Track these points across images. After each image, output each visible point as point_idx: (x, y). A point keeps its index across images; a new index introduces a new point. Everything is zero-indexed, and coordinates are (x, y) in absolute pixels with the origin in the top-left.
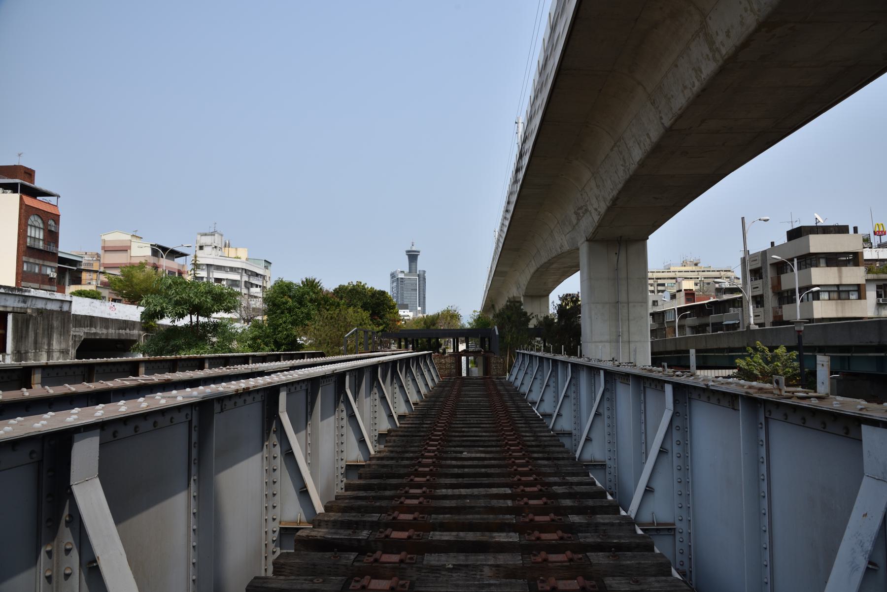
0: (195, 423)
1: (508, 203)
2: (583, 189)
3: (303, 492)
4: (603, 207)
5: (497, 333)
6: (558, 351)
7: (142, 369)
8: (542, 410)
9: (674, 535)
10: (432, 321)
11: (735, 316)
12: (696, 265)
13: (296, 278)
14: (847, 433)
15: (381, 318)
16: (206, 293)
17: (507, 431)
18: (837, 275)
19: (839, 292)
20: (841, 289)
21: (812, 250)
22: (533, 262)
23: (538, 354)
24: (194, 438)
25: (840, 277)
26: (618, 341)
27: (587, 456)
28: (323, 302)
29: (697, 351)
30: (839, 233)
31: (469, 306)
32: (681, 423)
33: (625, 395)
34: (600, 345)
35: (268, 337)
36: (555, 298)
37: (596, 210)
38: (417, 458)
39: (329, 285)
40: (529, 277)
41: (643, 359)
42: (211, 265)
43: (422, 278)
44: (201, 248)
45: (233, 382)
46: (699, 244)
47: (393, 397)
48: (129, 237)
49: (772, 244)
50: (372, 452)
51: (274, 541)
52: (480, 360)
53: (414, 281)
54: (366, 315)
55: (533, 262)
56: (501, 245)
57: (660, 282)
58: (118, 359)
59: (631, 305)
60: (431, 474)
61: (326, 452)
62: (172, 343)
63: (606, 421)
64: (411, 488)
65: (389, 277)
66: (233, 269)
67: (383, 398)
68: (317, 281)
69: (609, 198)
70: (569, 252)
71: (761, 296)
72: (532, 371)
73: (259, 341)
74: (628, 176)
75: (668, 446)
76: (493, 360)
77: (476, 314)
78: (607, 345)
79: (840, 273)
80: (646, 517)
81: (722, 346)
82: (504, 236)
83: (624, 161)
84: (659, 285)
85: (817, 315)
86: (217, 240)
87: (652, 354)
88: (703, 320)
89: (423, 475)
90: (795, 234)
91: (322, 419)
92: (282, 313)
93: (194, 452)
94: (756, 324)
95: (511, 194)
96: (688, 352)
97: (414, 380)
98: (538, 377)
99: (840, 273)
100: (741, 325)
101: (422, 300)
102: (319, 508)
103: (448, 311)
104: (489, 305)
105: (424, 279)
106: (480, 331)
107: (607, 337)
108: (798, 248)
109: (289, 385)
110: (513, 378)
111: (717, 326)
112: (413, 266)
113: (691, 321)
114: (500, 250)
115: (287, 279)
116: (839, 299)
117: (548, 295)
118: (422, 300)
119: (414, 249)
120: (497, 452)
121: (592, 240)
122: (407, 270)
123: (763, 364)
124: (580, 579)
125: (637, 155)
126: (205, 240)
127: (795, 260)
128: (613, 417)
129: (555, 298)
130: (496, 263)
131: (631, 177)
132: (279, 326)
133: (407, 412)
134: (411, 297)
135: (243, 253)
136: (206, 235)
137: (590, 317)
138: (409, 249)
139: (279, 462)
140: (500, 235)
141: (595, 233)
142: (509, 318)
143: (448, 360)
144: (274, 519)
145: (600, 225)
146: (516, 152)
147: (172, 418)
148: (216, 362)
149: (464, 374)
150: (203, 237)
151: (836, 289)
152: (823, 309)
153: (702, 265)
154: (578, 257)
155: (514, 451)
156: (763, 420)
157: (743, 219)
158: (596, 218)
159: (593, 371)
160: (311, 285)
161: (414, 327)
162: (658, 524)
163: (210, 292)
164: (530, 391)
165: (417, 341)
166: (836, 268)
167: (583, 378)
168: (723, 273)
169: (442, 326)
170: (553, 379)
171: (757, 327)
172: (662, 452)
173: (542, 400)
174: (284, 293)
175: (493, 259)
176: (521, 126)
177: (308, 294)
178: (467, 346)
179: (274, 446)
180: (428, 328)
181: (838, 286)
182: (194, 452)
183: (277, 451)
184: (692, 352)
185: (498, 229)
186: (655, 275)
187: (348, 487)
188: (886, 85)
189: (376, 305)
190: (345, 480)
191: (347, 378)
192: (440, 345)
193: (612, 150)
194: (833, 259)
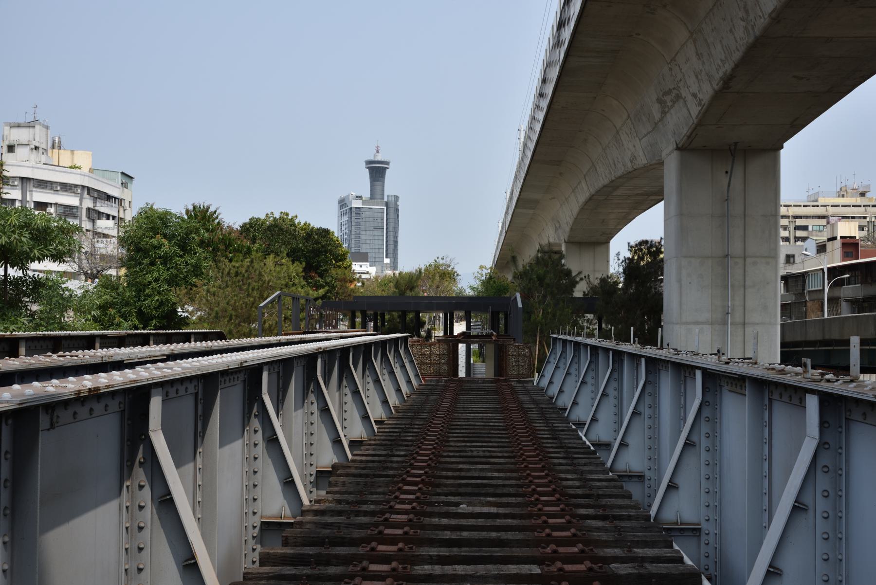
1: (544, 81)
4: (707, 92)
5: (520, 305)
12: (863, 194)
15: (321, 276)
16: (21, 227)
17: (535, 469)
22: (583, 184)
26: (725, 323)
28: (222, 247)
29: (863, 342)
31: (472, 263)
33: (736, 412)
35: (127, 304)
36: (620, 247)
37: (694, 95)
38: (383, 513)
40: (576, 210)
41: (763, 349)
42: (29, 179)
43: (392, 208)
44: (11, 148)
45: (71, 379)
47: (342, 410)
50: (306, 502)
55: (583, 184)
56: (529, 154)
57: (799, 222)
59: (748, 260)
60: (406, 539)
63: (704, 455)
64: (372, 562)
65: (336, 206)
66: (66, 187)
67: (325, 410)
68: (212, 209)
69: (718, 76)
70: (647, 169)
72: (565, 364)
73: (112, 311)
74: (751, 39)
75: (807, 500)
76: (511, 351)
77: (485, 271)
78: (707, 328)
82: (535, 138)
83: (747, 12)
84: (798, 228)
86: (38, 135)
89: (393, 541)
92: (152, 264)
95: (549, 65)
97: (377, 381)
101: (391, 247)
103: (437, 266)
104: (507, 256)
105: (397, 210)
106: (490, 302)
109: (166, 385)
110: (545, 382)
112: (379, 188)
113: (851, 291)
114: (527, 162)
115: (160, 205)
117: (607, 242)
118: (391, 247)
119: (379, 158)
120: (517, 505)
122: (366, 194)
126: (16, 136)
128: (715, 450)
129: (620, 247)
133: (364, 435)
135: (84, 159)
136: (19, 126)
137: (680, 281)
138: (371, 158)
139: (148, 516)
140: (528, 137)
141: (690, 137)
142: (541, 279)
143: (436, 350)
145: (701, 123)
146: (537, 76)
147: (75, 413)
148: (38, 345)
149: (462, 374)
150: (15, 131)
154: (662, 177)
158: (695, 110)
159: (683, 370)
160: (202, 216)
161: (379, 293)
162: (682, 524)
163: (27, 225)
164: (575, 403)
165: (383, 316)
169: (425, 291)
172: (798, 508)
173: (594, 420)
174: (155, 230)
175: (522, 159)
177: (197, 231)
178: (468, 327)
179: (141, 487)
180: (402, 293)
185: (524, 126)
186: (792, 211)
187: (265, 560)
189: (315, 252)
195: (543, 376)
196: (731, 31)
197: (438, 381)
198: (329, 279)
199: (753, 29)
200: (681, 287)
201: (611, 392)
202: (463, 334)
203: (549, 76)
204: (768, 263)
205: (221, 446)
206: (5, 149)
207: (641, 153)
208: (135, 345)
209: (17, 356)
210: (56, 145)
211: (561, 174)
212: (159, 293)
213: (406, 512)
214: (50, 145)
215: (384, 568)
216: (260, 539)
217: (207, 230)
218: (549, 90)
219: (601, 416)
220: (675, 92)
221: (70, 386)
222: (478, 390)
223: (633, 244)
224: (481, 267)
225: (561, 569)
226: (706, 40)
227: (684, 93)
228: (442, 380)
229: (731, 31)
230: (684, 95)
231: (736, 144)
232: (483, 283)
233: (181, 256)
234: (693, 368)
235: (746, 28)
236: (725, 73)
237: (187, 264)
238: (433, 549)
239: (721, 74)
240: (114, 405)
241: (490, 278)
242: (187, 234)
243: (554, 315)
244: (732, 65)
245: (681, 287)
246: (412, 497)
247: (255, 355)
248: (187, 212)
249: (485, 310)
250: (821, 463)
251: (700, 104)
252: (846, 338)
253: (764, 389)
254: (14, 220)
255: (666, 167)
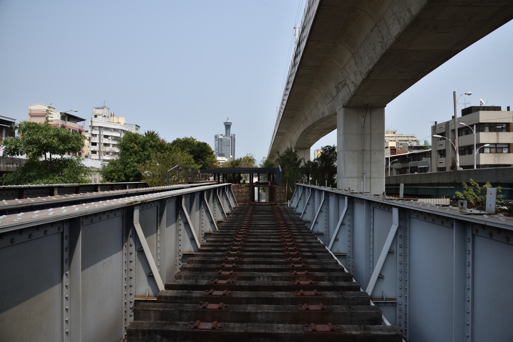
0: (66, 233)
1: (288, 83)
2: (344, 68)
3: (151, 276)
4: (359, 79)
5: (281, 170)
6: (322, 184)
7: (56, 192)
8: (335, 250)
9: (396, 306)
10: (235, 163)
11: (426, 163)
12: (394, 133)
13: (181, 137)
14: (491, 237)
15: (203, 160)
16: (54, 136)
17: (287, 238)
18: (496, 137)
19: (496, 148)
20: (498, 146)
21: (480, 122)
22: (302, 126)
23: (301, 184)
24: (66, 243)
25: (498, 138)
27: (315, 230)
28: (159, 148)
29: (405, 185)
30: (495, 110)
31: (260, 156)
32: (403, 233)
33: (360, 213)
34: (351, 180)
35: (120, 171)
37: (353, 82)
38: (232, 241)
39: (168, 137)
40: (298, 135)
41: (378, 189)
43: (233, 139)
44: (96, 116)
45: (126, 198)
46: (412, 116)
47: (214, 210)
48: (47, 108)
49: (436, 122)
50: (199, 246)
51: (131, 308)
52: (267, 189)
53: (228, 141)
54: (191, 157)
55: (302, 126)
56: (281, 114)
58: (25, 185)
59: (372, 152)
60: (234, 269)
61: (164, 252)
62: (28, 174)
64: (229, 257)
65: (214, 138)
66: (115, 130)
67: (207, 211)
68: (155, 133)
69: (365, 71)
70: (329, 117)
71: (444, 151)
73: (114, 174)
74: (384, 51)
76: (277, 190)
77: (265, 159)
78: (356, 179)
79: (498, 135)
80: (378, 294)
81: (432, 182)
82: (284, 107)
83: (383, 38)
85: (482, 163)
86: (105, 112)
87: (386, 185)
88: (405, 165)
89: (228, 269)
90: (466, 112)
91: (167, 227)
92: (131, 155)
93: (159, 218)
94: (461, 167)
95: (290, 76)
96: (399, 185)
97: (227, 199)
98: (302, 198)
99: (498, 135)
100: (430, 168)
101: (233, 152)
102: (199, 246)
103: (247, 157)
104: (271, 156)
106: (267, 169)
107: (355, 175)
108: (470, 119)
109: (143, 204)
111: (414, 169)
113: (398, 165)
114: (281, 117)
116: (496, 152)
117: (310, 148)
118: (233, 152)
119: (228, 121)
120: (282, 263)
121: (348, 106)
122: (224, 134)
123: (476, 196)
124: (330, 324)
125: (396, 29)
126: (98, 112)
127: (475, 126)
130: (278, 127)
131: (387, 51)
132: (128, 164)
133: (222, 219)
134: (226, 149)
135: (122, 120)
136: (99, 108)
137: (344, 161)
139: (134, 256)
141: (350, 101)
142: (288, 160)
143: (244, 190)
144: (131, 294)
145: (355, 95)
146: (285, 83)
147: (100, 218)
148: (63, 190)
149: (256, 198)
150: (97, 110)
151: (494, 146)
152: (486, 159)
153: (398, 133)
155: (287, 242)
156: (470, 237)
157: (454, 93)
158: (353, 89)
159: (339, 196)
160: (151, 136)
161: (227, 167)
162: (386, 299)
163: (58, 135)
164: (297, 206)
165: (226, 175)
166: (495, 133)
167: (332, 201)
168: (410, 138)
169: (243, 165)
170: (325, 206)
171: (462, 169)
173: (305, 213)
175: (278, 120)
176: (297, 30)
177: (149, 142)
178: (259, 179)
180: (234, 167)
181: (496, 144)
182: (159, 218)
183: (133, 249)
184: (402, 186)
185: (279, 106)
187: (183, 269)
188: (512, 26)
189: (199, 152)
190: (181, 263)
191: (183, 200)
192: (241, 178)
193: (372, 31)
194: (493, 127)
195: (292, 202)
196: (373, 49)
197: (245, 205)
198: (206, 162)
199: (385, 45)
200: (345, 163)
201: (311, 203)
202: (256, 182)
203: (290, 80)
204: (380, 153)
205: (167, 227)
206: (93, 116)
207: (327, 111)
208: (143, 187)
209: (126, 189)
210: (112, 115)
211: (293, 122)
212: (133, 167)
213: (235, 256)
214: (110, 115)
215: (231, 266)
216: (182, 260)
217: (154, 141)
218: (290, 86)
219: (299, 205)
220: (344, 82)
221: (126, 200)
222: (263, 211)
223: (323, 147)
224: (264, 158)
225: (296, 274)
226: (360, 56)
227: (348, 82)
228: (247, 207)
229: (373, 49)
230: (348, 83)
231: (368, 104)
232: (264, 164)
233: (142, 152)
234: (343, 196)
235: (382, 46)
236: (369, 70)
237: (145, 155)
238: (244, 292)
239: (367, 70)
240: (119, 213)
241: (267, 161)
242: (145, 142)
243: (294, 175)
244: (373, 65)
245: (345, 163)
246: (240, 239)
247: (87, 207)
248: (146, 134)
249: (266, 173)
250: (399, 235)
251: (355, 86)
252: (398, 183)
253: (371, 205)
254: (51, 132)
255: (338, 116)
